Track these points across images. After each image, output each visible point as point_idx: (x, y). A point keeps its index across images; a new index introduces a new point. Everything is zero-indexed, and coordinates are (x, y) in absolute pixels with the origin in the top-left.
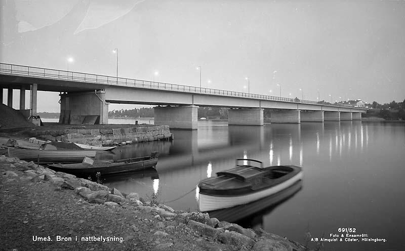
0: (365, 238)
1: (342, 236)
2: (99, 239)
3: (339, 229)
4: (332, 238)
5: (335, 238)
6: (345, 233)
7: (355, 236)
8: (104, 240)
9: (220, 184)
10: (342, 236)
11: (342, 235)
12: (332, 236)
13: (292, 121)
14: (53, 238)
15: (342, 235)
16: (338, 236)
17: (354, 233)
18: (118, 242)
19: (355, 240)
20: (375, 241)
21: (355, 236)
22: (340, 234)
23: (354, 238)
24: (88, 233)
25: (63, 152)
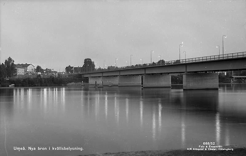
0: (221, 148)
1: (207, 147)
2: (67, 149)
3: (204, 143)
4: (200, 148)
5: (202, 148)
6: (208, 146)
7: (214, 147)
8: (32, 149)
9: (117, 104)
10: (207, 147)
11: (207, 146)
12: (200, 147)
13: (211, 87)
14: (27, 148)
15: (207, 146)
16: (204, 147)
17: (214, 146)
18: (79, 151)
19: (214, 149)
20: (227, 150)
21: (214, 147)
22: (205, 145)
23: (214, 148)
24: (222, 151)
25: (29, 97)
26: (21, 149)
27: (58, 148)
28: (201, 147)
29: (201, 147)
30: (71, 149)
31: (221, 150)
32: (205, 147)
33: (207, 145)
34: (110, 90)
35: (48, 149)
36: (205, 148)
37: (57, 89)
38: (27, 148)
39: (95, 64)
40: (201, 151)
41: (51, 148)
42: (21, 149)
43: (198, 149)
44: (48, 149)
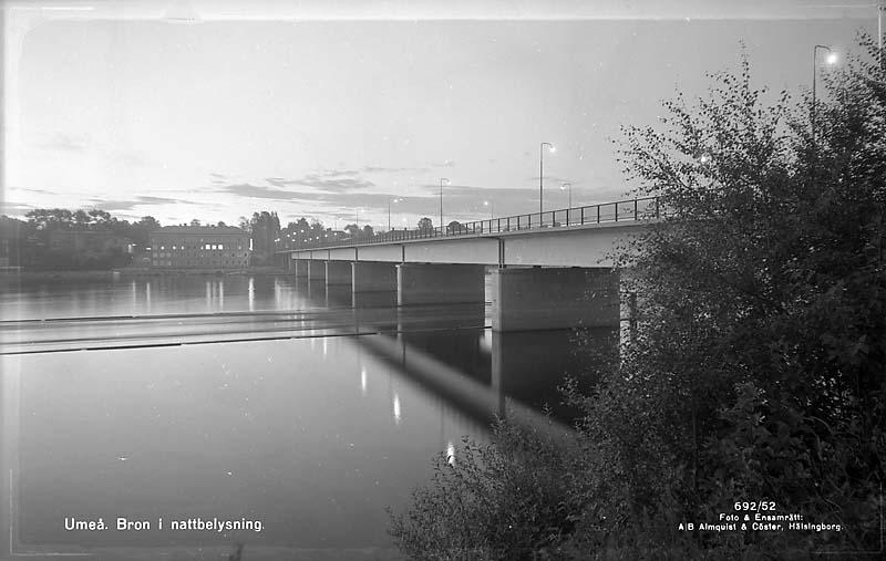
1: (747, 518)
4: (724, 522)
5: (731, 523)
6: (752, 514)
10: (747, 518)
16: (737, 518)
17: (772, 513)
21: (774, 519)
22: (742, 513)
23: (772, 522)
26: (92, 525)
27: (798, 528)
28: (728, 518)
29: (728, 518)
30: (221, 527)
31: (798, 528)
32: (742, 517)
33: (749, 512)
34: (22, 328)
35: (154, 524)
36: (742, 521)
37: (221, 284)
38: (111, 523)
39: (57, 207)
40: (727, 531)
41: (167, 524)
42: (92, 525)
43: (718, 528)
44: (154, 524)
